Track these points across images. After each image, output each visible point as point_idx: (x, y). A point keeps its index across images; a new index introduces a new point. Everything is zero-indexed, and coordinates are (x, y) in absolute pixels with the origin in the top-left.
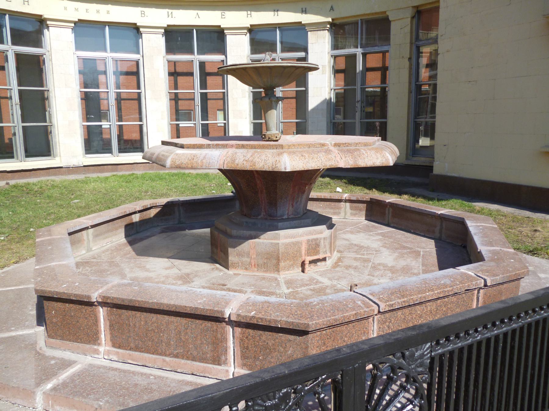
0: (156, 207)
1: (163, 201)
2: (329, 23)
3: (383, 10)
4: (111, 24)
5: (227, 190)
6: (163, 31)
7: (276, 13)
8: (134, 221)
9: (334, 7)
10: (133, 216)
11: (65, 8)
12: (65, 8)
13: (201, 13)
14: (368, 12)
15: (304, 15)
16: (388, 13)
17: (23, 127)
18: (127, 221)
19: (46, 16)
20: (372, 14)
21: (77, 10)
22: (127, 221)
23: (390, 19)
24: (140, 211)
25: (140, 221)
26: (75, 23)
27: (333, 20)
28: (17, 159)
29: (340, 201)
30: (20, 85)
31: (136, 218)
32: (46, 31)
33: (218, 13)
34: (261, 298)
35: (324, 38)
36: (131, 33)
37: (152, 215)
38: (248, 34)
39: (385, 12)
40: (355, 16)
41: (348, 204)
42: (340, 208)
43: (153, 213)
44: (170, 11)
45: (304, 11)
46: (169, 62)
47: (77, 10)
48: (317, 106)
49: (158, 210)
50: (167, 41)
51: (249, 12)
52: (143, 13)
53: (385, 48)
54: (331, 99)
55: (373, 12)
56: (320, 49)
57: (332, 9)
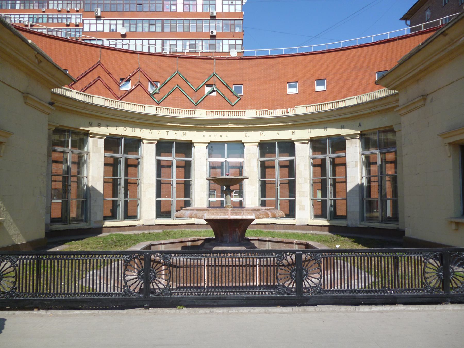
0: (201, 240)
1: (205, 238)
2: (358, 134)
3: (391, 125)
4: (228, 142)
5: (210, 233)
6: (257, 144)
7: (326, 129)
8: (188, 245)
9: (361, 124)
10: (187, 243)
11: (204, 136)
12: (204, 136)
13: (280, 132)
14: (382, 126)
15: (343, 130)
16: (394, 127)
17: (326, 176)
18: (184, 244)
19: (193, 141)
20: (385, 127)
21: (210, 136)
22: (184, 244)
23: (395, 130)
24: (191, 241)
25: (191, 246)
26: (209, 143)
27: (361, 132)
28: (119, 219)
29: (265, 241)
30: (177, 178)
31: (189, 244)
32: (193, 148)
33: (290, 132)
34: (287, 296)
35: (356, 143)
36: (242, 145)
37: (199, 244)
38: (309, 143)
39: (391, 126)
40: (374, 129)
41: (270, 243)
42: (265, 245)
43: (200, 243)
44: (262, 132)
45: (343, 127)
46: (261, 162)
47: (210, 136)
48: (353, 189)
49: (202, 242)
50: (260, 149)
51: (309, 130)
52: (246, 135)
53: (394, 149)
54: (362, 184)
55: (385, 126)
56: (354, 151)
57: (360, 125)
